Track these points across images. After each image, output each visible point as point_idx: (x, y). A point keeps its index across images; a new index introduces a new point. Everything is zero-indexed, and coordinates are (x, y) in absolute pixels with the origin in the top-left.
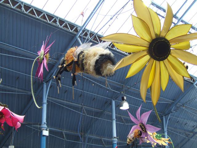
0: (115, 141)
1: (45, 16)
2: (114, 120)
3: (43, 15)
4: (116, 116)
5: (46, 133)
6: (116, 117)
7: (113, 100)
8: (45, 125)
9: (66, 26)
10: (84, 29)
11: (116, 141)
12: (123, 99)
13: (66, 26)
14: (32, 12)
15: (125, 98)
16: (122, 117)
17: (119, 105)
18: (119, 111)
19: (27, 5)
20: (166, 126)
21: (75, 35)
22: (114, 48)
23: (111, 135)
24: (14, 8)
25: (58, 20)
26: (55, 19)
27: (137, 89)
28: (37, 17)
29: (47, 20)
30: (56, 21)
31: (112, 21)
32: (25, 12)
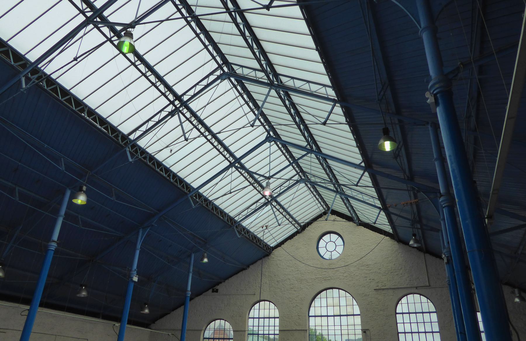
0: (52, 245)
1: (108, 128)
2: (61, 216)
3: (117, 134)
4: (66, 211)
5: (135, 279)
6: (66, 214)
7: (69, 189)
8: (136, 272)
9: (69, 101)
10: (35, 67)
11: (55, 247)
12: (81, 190)
13: (145, 158)
14: (55, 90)
15: (84, 188)
16: (80, 216)
17: (74, 196)
18: (71, 204)
19: (112, 127)
20: (140, 242)
21: (19, 72)
22: (82, 114)
23: (49, 238)
24: (76, 110)
25: (148, 157)
26: (118, 134)
27: (120, 189)
28: (74, 109)
29: (73, 106)
30: (118, 137)
31: (75, 62)
32: (46, 88)
